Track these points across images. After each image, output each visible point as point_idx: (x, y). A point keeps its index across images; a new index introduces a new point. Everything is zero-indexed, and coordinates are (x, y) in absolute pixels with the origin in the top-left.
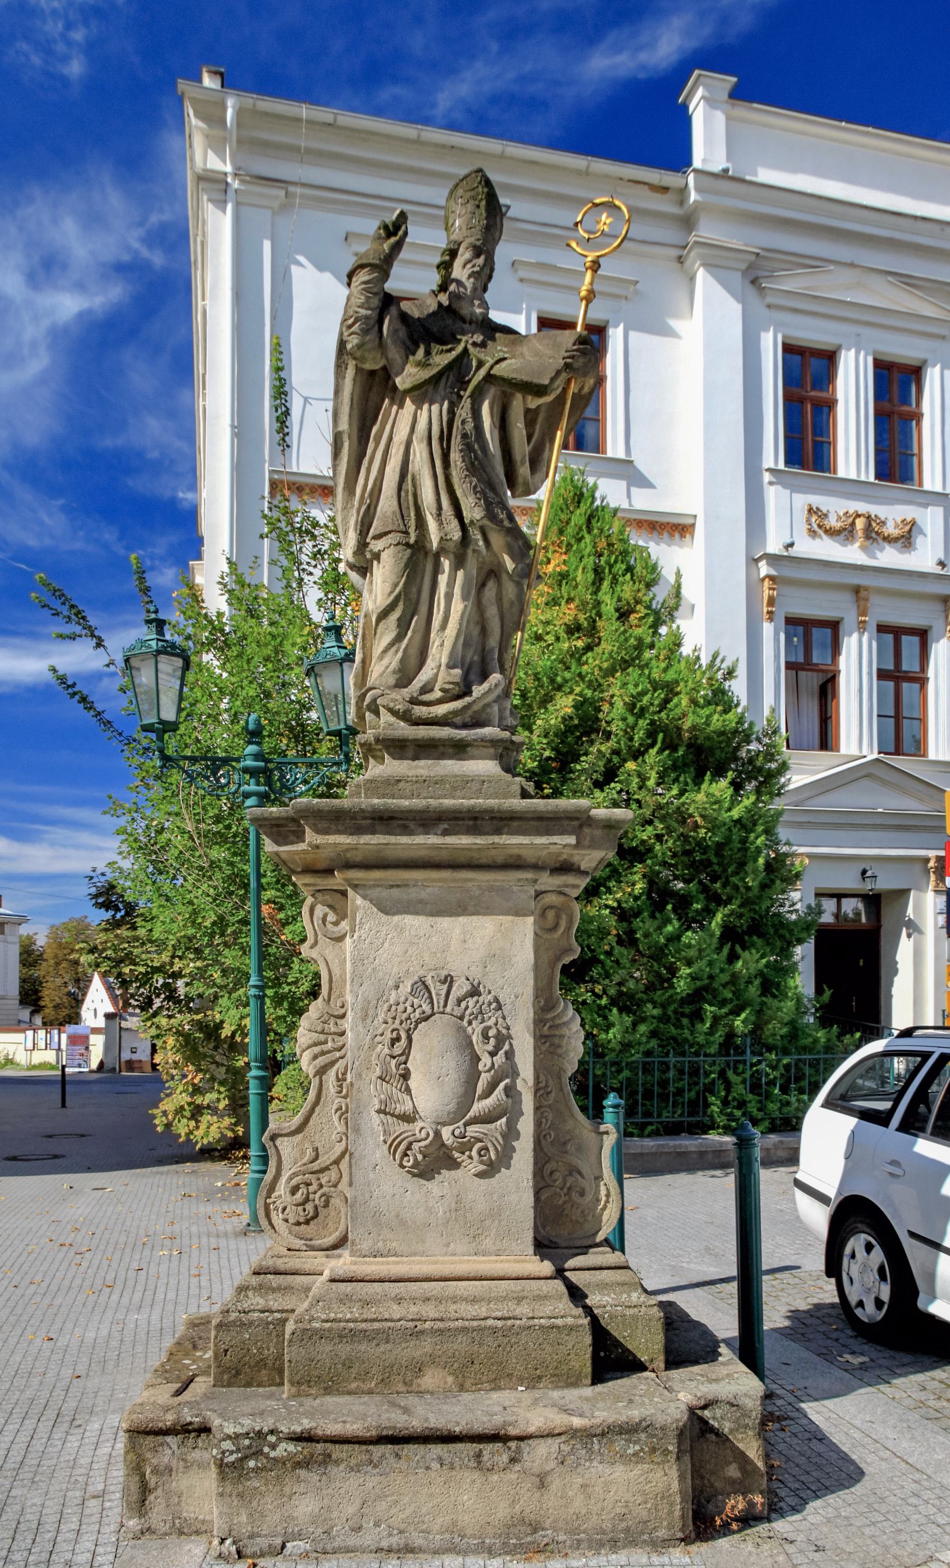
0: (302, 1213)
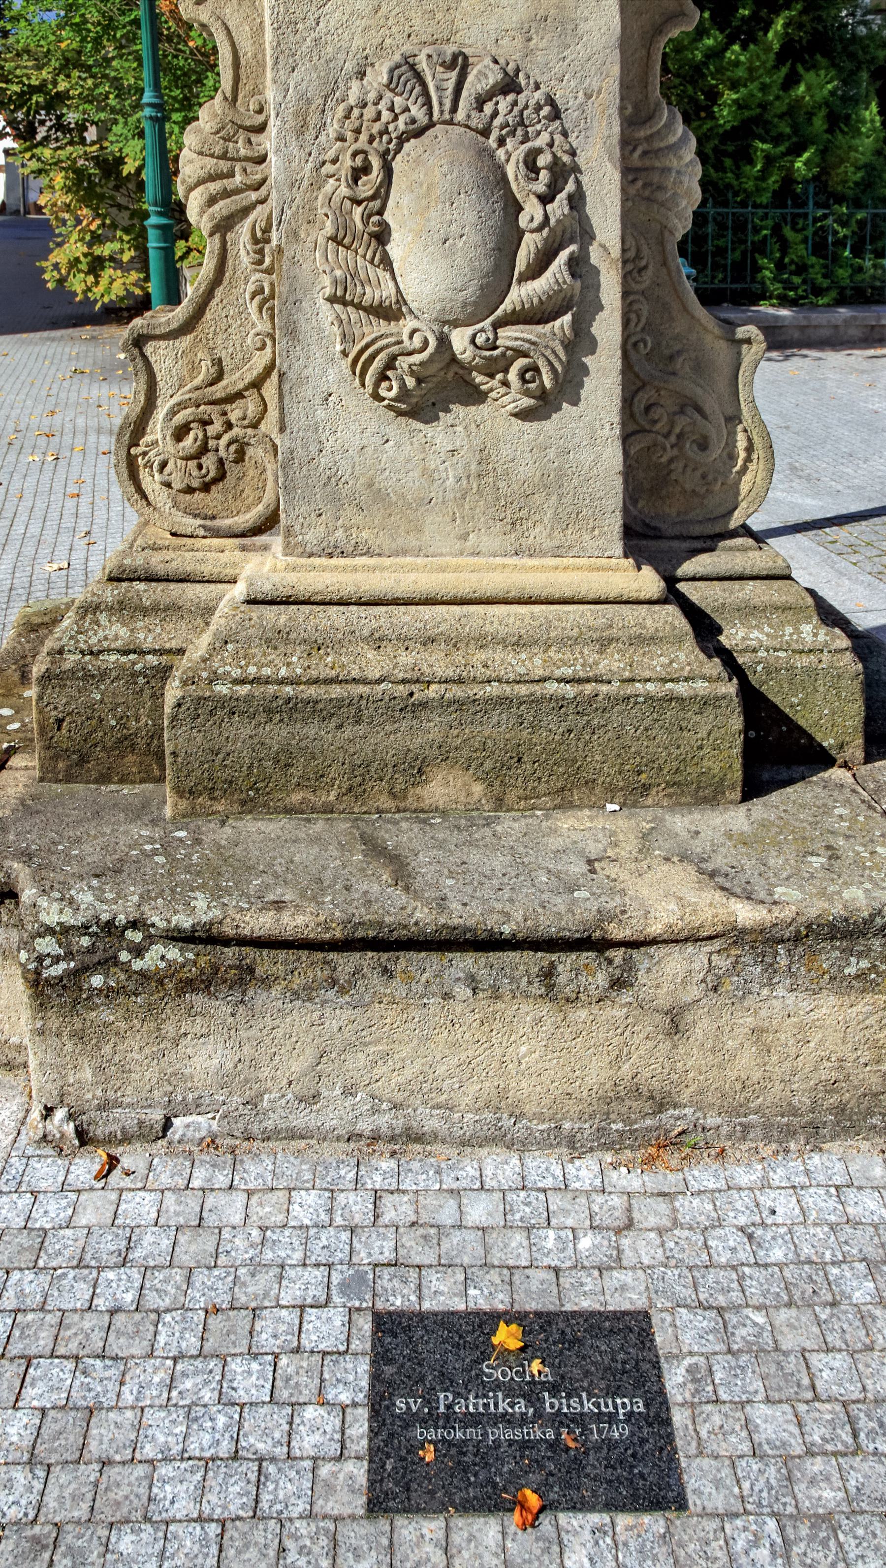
0: (195, 473)
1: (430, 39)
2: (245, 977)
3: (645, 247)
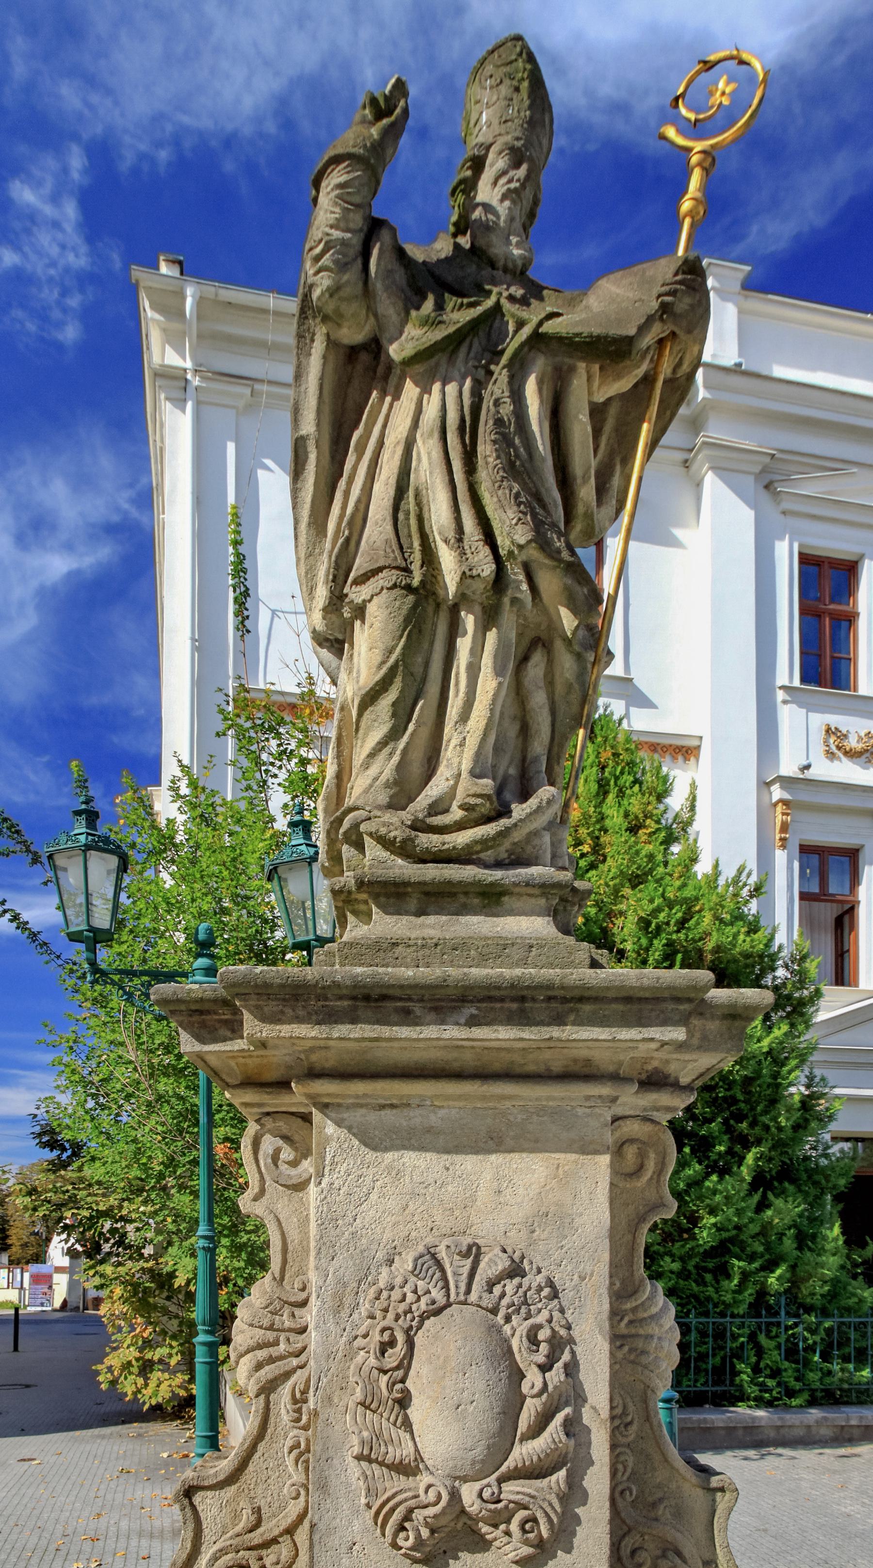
1: (449, 1232)
3: (631, 1404)
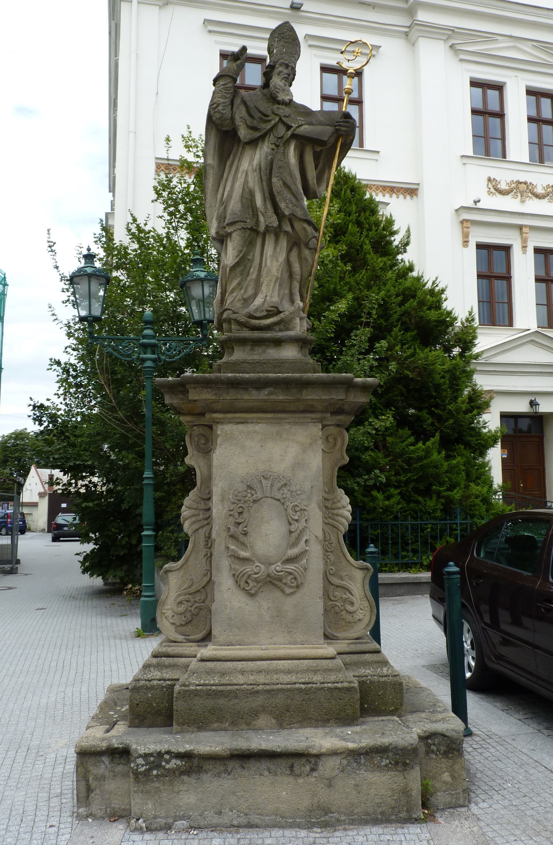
0: (184, 619)
2: (200, 770)
